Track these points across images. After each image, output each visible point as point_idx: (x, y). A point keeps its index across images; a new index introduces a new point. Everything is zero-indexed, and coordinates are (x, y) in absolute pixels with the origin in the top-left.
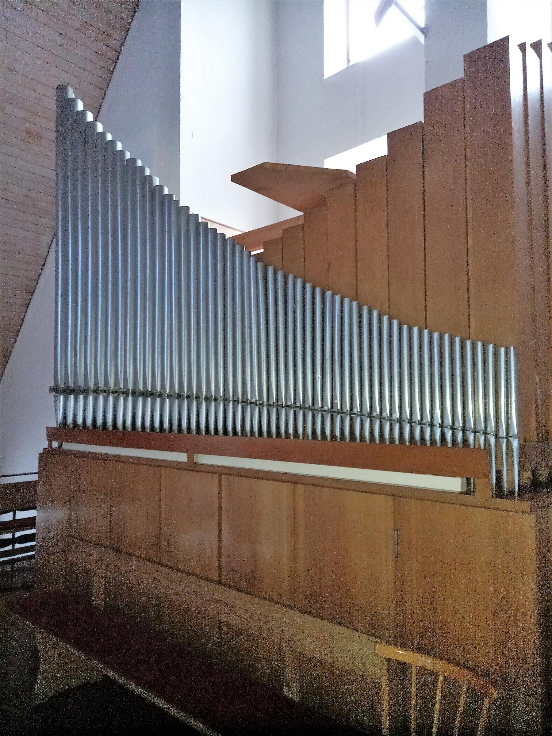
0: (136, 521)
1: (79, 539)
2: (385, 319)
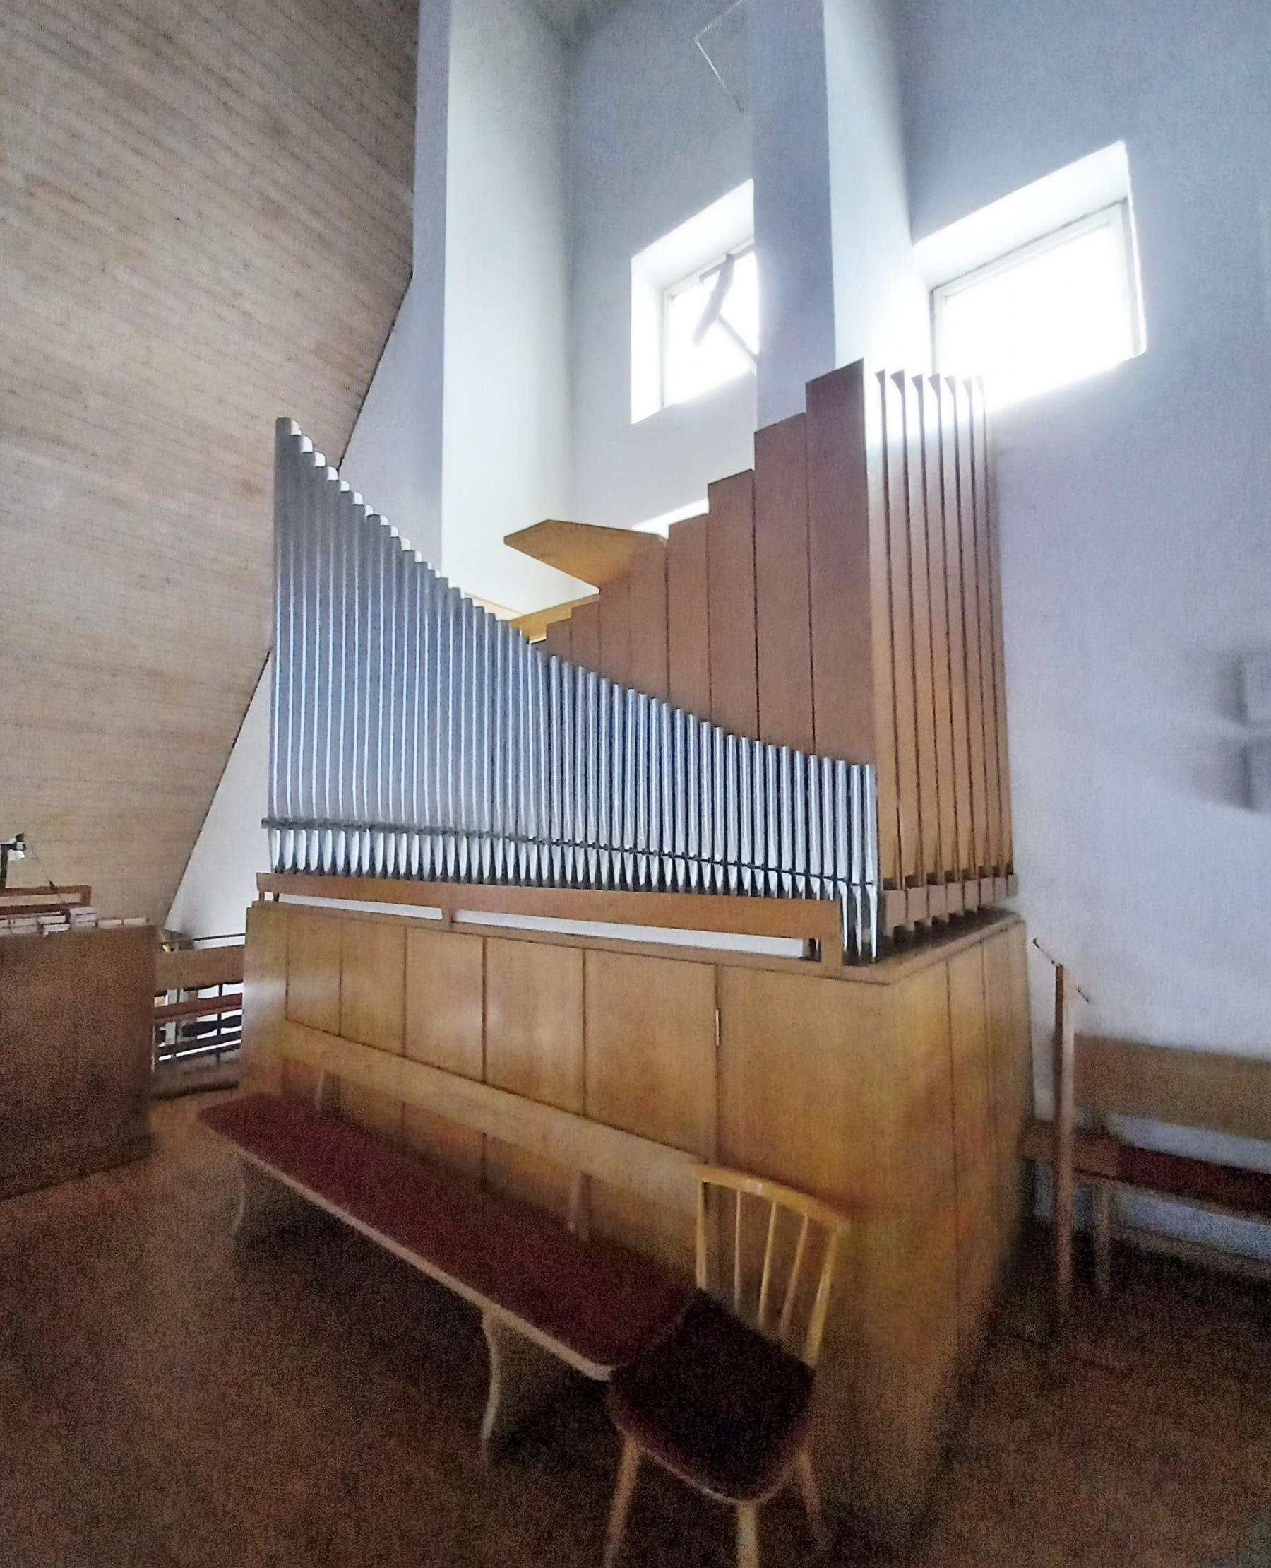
0: (373, 997)
1: (299, 1023)
2: (705, 726)
